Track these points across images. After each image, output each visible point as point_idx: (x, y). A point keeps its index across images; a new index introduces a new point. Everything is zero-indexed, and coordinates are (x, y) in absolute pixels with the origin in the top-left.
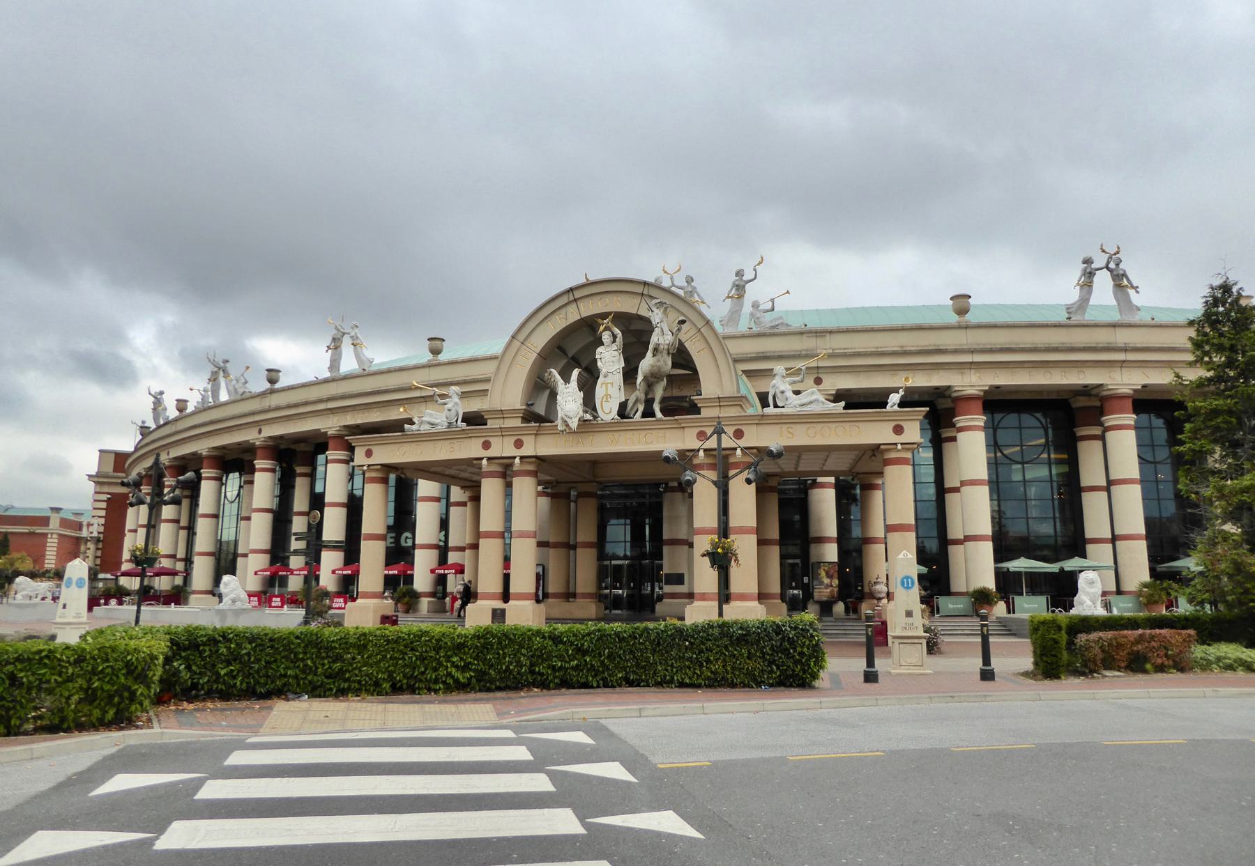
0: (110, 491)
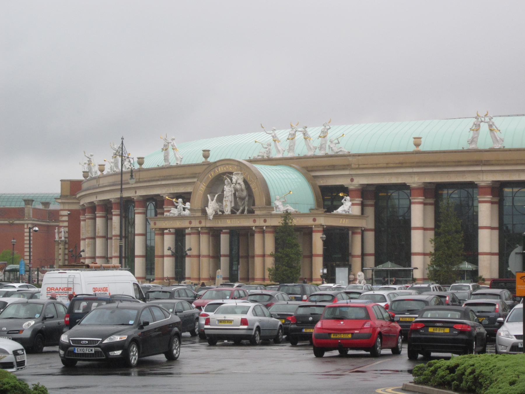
0: (70, 209)
